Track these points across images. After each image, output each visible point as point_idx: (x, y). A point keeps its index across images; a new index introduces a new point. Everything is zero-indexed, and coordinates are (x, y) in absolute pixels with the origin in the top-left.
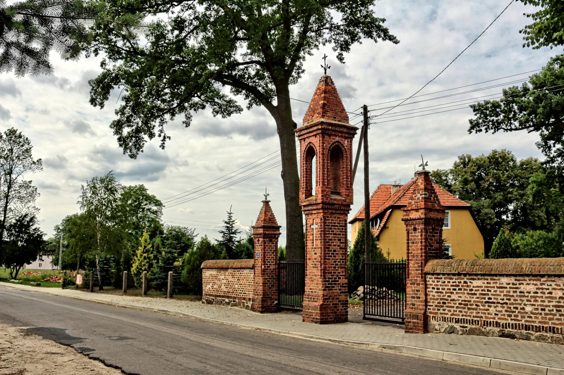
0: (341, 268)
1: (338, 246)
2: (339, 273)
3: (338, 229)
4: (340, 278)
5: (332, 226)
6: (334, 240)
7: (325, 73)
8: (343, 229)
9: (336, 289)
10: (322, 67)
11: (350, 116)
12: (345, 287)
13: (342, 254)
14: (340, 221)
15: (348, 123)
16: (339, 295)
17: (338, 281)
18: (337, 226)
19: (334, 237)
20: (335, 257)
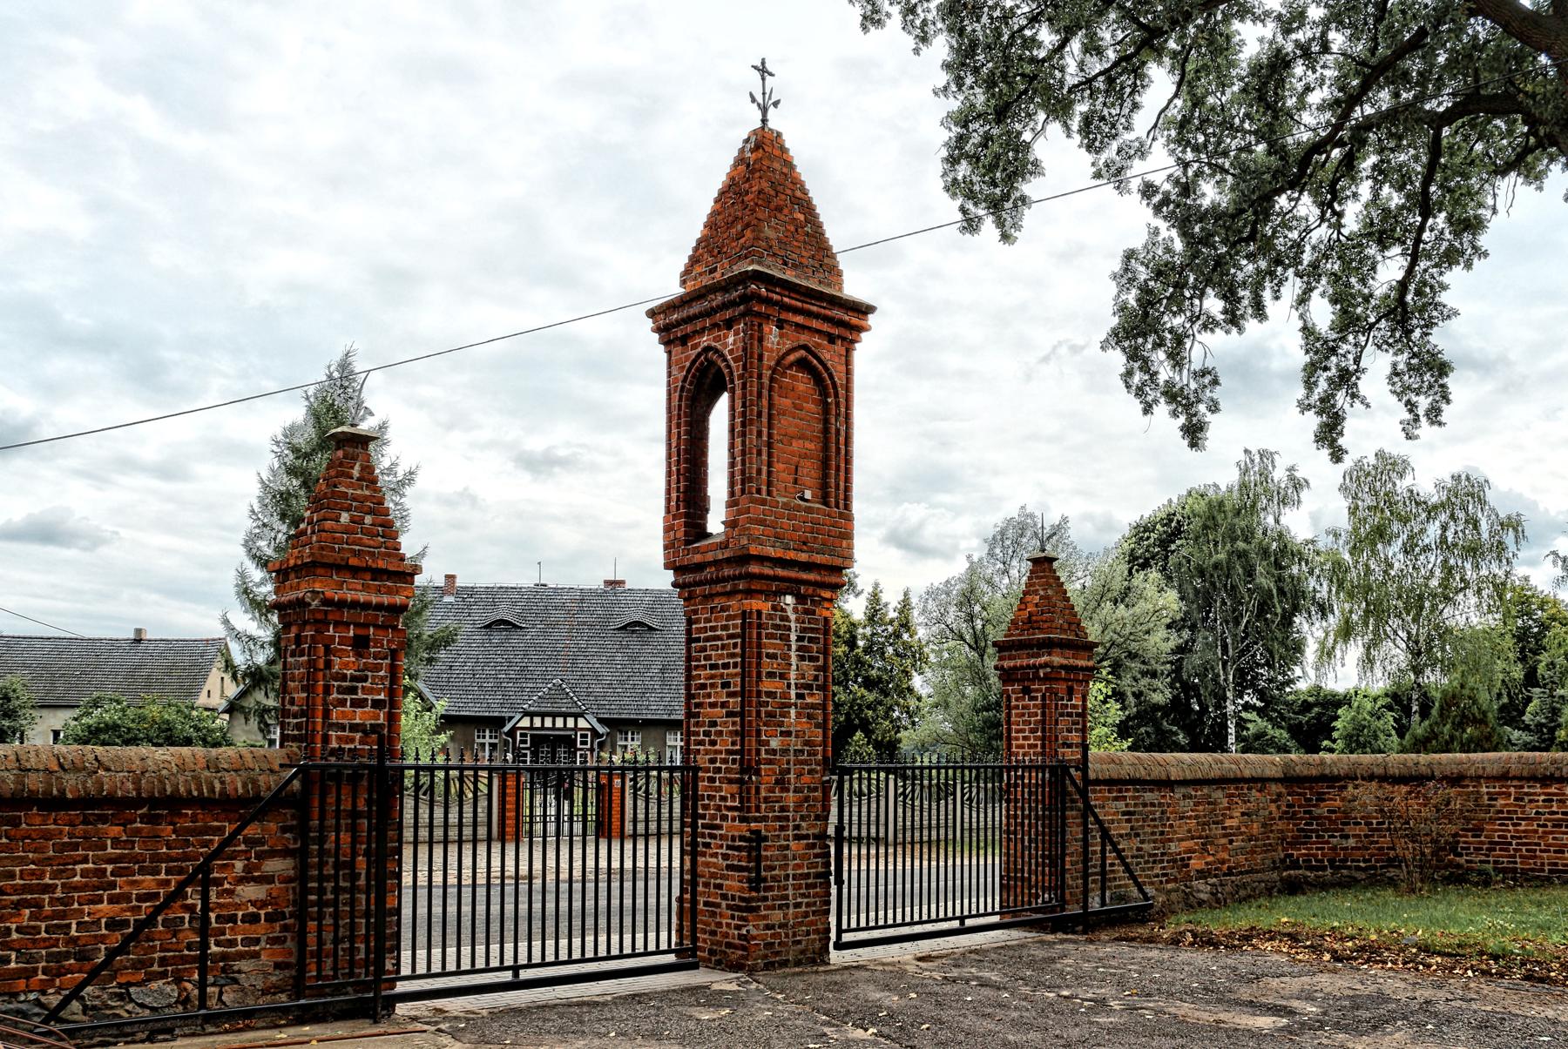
0: (730, 781)
1: (724, 705)
2: (723, 799)
3: (723, 647)
4: (724, 818)
5: (707, 639)
6: (713, 686)
7: (764, 121)
8: (735, 645)
9: (715, 855)
10: (753, 100)
11: (843, 262)
12: (738, 849)
13: (732, 733)
14: (729, 618)
15: (840, 289)
16: (723, 877)
17: (719, 827)
18: (719, 638)
19: (712, 677)
20: (713, 743)
